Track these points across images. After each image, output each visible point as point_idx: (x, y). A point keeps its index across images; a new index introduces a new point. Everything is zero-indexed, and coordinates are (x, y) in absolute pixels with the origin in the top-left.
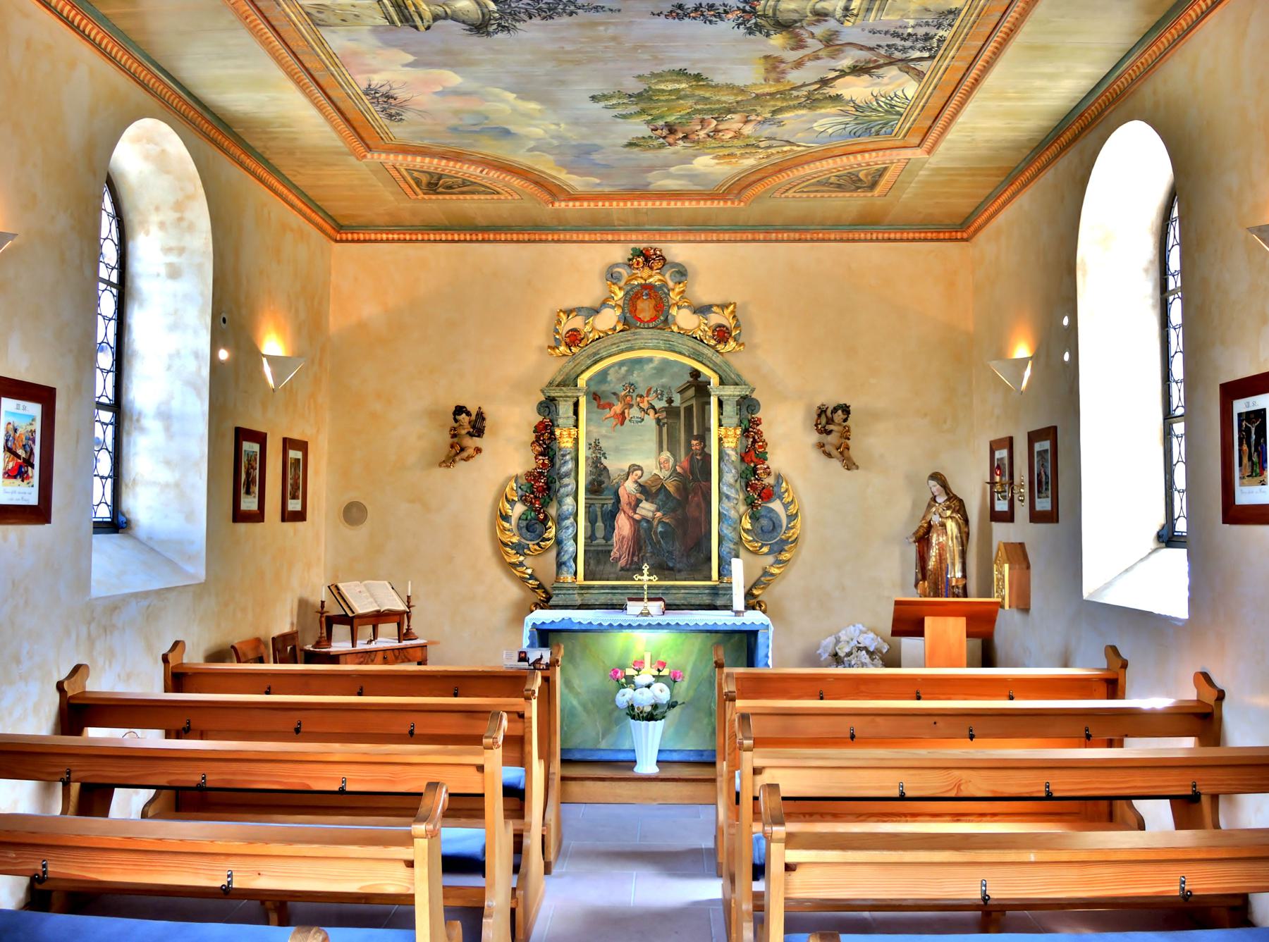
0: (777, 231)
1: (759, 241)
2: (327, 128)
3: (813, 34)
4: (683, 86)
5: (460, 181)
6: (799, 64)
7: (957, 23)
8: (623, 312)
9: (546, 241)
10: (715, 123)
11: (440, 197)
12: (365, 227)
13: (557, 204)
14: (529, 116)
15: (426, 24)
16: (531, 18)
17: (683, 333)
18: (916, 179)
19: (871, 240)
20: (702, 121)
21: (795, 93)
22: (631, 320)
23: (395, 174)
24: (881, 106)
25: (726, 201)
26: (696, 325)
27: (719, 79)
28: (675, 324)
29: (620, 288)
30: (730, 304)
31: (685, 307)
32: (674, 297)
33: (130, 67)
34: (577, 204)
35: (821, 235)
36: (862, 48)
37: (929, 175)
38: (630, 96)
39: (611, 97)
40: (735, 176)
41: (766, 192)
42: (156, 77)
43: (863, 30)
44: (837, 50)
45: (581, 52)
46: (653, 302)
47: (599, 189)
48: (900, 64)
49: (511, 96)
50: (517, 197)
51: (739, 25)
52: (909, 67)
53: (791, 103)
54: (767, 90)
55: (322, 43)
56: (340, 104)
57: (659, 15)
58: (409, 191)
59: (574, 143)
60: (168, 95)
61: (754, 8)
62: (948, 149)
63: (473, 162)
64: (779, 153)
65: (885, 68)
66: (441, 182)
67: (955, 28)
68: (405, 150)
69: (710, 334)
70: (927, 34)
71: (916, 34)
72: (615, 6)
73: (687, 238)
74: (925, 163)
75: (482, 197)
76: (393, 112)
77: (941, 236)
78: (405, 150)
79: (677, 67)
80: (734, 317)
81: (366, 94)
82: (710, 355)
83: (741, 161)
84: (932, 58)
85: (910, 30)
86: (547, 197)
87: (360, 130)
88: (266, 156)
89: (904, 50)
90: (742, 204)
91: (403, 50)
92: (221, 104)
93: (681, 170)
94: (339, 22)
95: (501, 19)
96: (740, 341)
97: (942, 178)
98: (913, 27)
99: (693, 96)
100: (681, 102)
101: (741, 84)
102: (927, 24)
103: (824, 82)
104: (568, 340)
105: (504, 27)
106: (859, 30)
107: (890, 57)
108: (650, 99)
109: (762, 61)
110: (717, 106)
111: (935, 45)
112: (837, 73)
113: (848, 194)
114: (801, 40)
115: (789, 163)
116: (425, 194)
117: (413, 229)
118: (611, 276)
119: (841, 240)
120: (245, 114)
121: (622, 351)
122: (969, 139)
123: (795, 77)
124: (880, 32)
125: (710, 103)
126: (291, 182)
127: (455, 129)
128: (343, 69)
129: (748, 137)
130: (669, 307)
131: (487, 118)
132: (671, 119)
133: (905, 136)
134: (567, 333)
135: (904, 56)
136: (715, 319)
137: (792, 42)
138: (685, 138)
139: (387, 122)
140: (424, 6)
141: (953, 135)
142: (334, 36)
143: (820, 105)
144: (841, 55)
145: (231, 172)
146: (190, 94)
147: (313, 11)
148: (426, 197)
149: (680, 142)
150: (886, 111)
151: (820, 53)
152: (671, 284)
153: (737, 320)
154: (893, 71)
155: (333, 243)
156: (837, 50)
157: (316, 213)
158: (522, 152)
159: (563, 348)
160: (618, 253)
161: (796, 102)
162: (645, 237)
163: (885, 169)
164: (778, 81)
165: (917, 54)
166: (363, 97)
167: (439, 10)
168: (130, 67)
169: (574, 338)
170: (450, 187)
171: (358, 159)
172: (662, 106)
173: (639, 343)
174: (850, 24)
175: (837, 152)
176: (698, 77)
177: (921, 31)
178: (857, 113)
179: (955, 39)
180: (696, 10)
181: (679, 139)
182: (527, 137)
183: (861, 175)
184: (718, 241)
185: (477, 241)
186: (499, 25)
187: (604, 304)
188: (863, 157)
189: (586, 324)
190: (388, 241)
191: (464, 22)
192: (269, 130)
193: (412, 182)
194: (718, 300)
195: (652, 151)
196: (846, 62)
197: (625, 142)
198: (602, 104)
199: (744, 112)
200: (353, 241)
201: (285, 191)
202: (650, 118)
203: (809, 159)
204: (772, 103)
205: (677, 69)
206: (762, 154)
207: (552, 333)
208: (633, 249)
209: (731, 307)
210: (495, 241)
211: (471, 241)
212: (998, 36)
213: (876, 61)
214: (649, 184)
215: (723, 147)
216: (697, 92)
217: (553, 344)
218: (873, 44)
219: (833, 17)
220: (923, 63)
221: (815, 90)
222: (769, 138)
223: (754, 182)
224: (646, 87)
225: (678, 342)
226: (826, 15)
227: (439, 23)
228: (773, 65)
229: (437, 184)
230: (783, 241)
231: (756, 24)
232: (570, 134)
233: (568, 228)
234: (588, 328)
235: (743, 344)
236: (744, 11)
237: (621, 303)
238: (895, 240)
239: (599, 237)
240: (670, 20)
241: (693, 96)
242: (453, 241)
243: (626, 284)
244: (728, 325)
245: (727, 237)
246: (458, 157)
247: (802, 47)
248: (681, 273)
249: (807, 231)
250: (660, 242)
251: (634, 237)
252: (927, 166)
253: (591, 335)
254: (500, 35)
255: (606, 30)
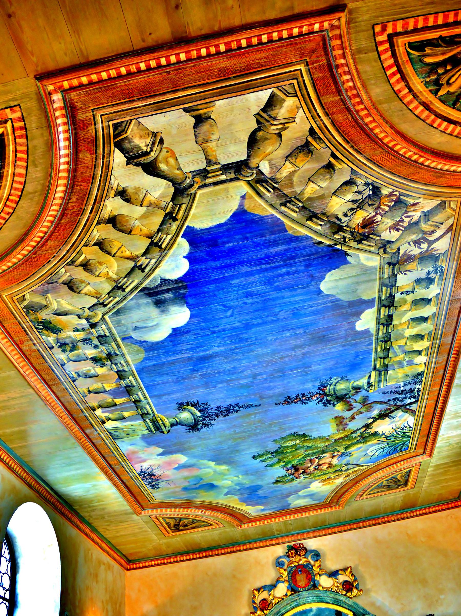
0: (362, 522)
1: (354, 529)
2: (121, 499)
3: (355, 400)
4: (298, 442)
5: (191, 521)
6: (352, 418)
7: (424, 380)
8: (290, 584)
9: (240, 551)
10: (317, 460)
11: (181, 533)
12: (142, 559)
13: (243, 526)
14: (222, 474)
15: (167, 429)
16: (218, 417)
17: (326, 590)
18: (428, 474)
19: (414, 516)
20: (311, 460)
21: (354, 435)
22: (295, 588)
23: (156, 521)
24: (398, 434)
25: (331, 507)
26: (332, 584)
27: (314, 434)
28: (320, 585)
29: (285, 570)
30: (348, 568)
31: (323, 574)
32: (316, 570)
33: (23, 476)
34: (254, 524)
35: (386, 519)
36: (381, 403)
37: (433, 470)
38: (272, 453)
39: (263, 455)
40: (332, 493)
41: (351, 498)
42: (36, 481)
43: (379, 393)
44: (370, 407)
45: (244, 432)
46: (305, 575)
47: (264, 513)
48: (402, 408)
49: (212, 464)
50: (221, 526)
51: (319, 402)
52: (407, 409)
53: (353, 441)
54: (340, 436)
55: (117, 448)
56: (128, 484)
57: (279, 404)
58: (164, 531)
59: (247, 486)
60: (58, 409)
61: (324, 392)
62: (439, 452)
63: (197, 507)
64: (354, 472)
65: (396, 412)
66: (181, 523)
67: (423, 383)
68: (161, 506)
69: (341, 587)
70: (411, 389)
71: (405, 390)
72: (257, 403)
73: (315, 535)
74: (429, 463)
75: (203, 529)
76: (154, 483)
77: (450, 506)
78: (161, 506)
79: (293, 431)
80: (352, 575)
81: (140, 475)
82: (344, 600)
83: (335, 481)
84: (417, 401)
85: (402, 388)
86: (237, 522)
87: (138, 498)
88: (90, 521)
89: (402, 400)
90: (341, 507)
91: (157, 446)
92: (68, 493)
93: (305, 492)
94: (125, 435)
95: (203, 420)
96: (360, 589)
97: (441, 471)
98: (403, 386)
99: (303, 446)
100: (298, 451)
101: (326, 436)
102: (410, 383)
103: (367, 426)
104: (261, 606)
105: (205, 424)
106: (377, 393)
107: (396, 405)
108: (282, 453)
109: (334, 420)
110: (316, 450)
111: (416, 394)
112: (372, 420)
113: (394, 491)
114: (351, 405)
115: (360, 478)
116: (173, 532)
117: (169, 556)
118: (279, 564)
119: (398, 520)
120: (80, 497)
121: (293, 608)
122: (448, 444)
123: (352, 426)
124: (388, 392)
125: (313, 450)
126: (103, 536)
127: (185, 489)
128: (128, 462)
129: (336, 466)
130: (315, 576)
131: (202, 479)
132: (294, 463)
133: (415, 449)
134: (260, 602)
135: (403, 403)
136: (342, 578)
137: (347, 407)
138: (304, 472)
139: (151, 490)
140: (166, 420)
141: (440, 443)
142: (123, 444)
143: (368, 440)
144: (372, 409)
145: (73, 532)
146: (52, 489)
147: (113, 432)
148: (174, 534)
149: (301, 475)
150: (402, 436)
151: (362, 410)
152: (312, 562)
153: (355, 576)
154: (399, 413)
155: (126, 571)
156: (370, 407)
157: (117, 554)
158: (222, 496)
159: (259, 612)
160: (280, 550)
161: (355, 441)
162: (293, 538)
163: (410, 471)
164: (344, 430)
165: (409, 401)
166: (139, 477)
167: (173, 421)
168: (23, 476)
169: (265, 605)
170: (186, 526)
171: (137, 515)
172: (289, 456)
173: (302, 601)
174: (372, 391)
175: (383, 466)
176: (304, 435)
177: (408, 388)
178: (388, 441)
179: (425, 389)
180: (297, 398)
181: (301, 474)
182: (223, 487)
183: (399, 478)
184: (333, 533)
185: (203, 557)
186: (203, 424)
187: (278, 581)
188: (397, 466)
189: (270, 595)
190: (155, 565)
191: (186, 425)
192: (91, 505)
193: (166, 526)
194: (341, 568)
195: (288, 484)
196: (375, 413)
197: (273, 481)
198: (259, 460)
199: (331, 451)
200: (137, 568)
201: (100, 542)
202: (284, 464)
203: (369, 473)
204: (344, 443)
205: (293, 433)
206: (345, 474)
207: (251, 604)
208: (287, 546)
209: (349, 569)
210: (213, 556)
211: (200, 558)
212: (446, 382)
213: (390, 409)
214: (290, 504)
215: (324, 474)
216: (305, 444)
217: (253, 611)
218: (386, 400)
219: (363, 388)
220: (413, 405)
221: (364, 431)
222: (347, 464)
223: (344, 493)
224: (279, 446)
225: (324, 596)
226: (360, 388)
227: (174, 428)
228: (340, 421)
229: (178, 525)
230: (367, 526)
231: (327, 400)
232: (244, 481)
233: (251, 541)
234: (271, 597)
235: (361, 590)
236: (320, 394)
237: (287, 579)
238: (427, 514)
239: (268, 543)
240: (285, 406)
241: (303, 446)
242: (190, 559)
243: (288, 567)
244: (350, 580)
245: (336, 530)
246: (188, 505)
247: (352, 408)
248: (317, 555)
249: (378, 518)
250: (301, 540)
251: (287, 540)
252: (431, 465)
253: (274, 602)
254: (204, 429)
255: (255, 417)
